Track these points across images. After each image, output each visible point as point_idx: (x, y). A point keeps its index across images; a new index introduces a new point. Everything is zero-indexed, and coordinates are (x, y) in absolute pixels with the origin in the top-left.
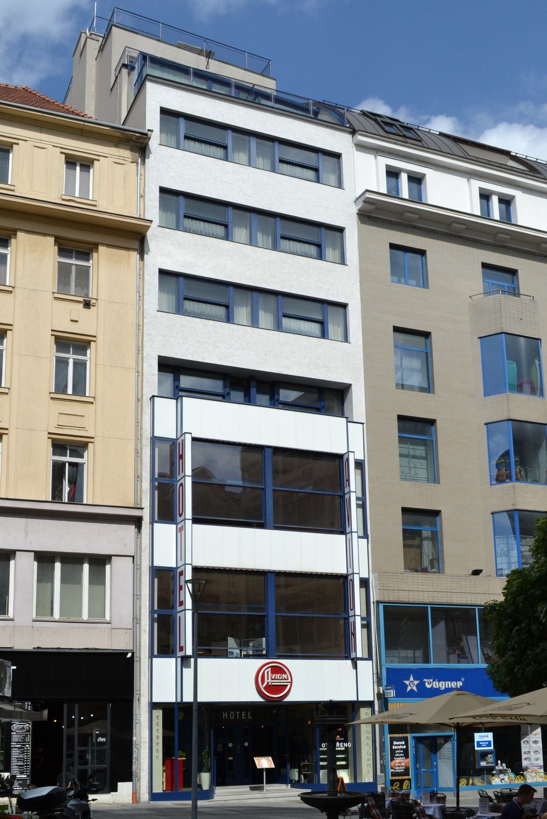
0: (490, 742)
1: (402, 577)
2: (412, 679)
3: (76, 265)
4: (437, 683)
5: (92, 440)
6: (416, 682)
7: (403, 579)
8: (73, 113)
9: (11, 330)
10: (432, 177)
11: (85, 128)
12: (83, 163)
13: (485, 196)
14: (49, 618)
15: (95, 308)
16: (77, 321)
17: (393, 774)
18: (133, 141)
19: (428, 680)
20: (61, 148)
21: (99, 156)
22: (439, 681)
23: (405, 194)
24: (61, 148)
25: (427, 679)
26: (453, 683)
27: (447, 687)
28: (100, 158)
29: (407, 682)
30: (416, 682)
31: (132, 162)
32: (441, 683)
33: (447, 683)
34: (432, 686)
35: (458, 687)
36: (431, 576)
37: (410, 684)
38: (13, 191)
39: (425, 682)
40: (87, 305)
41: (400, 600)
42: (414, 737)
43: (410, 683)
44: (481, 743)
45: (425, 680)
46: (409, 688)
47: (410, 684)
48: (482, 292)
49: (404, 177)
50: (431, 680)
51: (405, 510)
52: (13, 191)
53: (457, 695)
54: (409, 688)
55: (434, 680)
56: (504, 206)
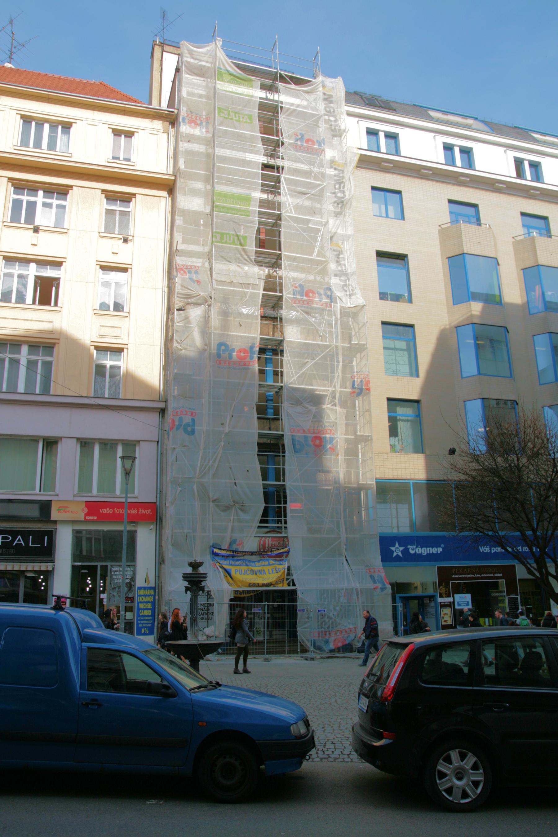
0: (468, 602)
1: (386, 457)
2: (397, 545)
3: (119, 211)
4: (420, 549)
5: (126, 346)
6: (401, 549)
7: (387, 458)
8: (136, 102)
9: (65, 262)
10: (404, 134)
11: (50, 97)
12: (127, 135)
13: (448, 148)
14: (89, 494)
15: (132, 243)
16: (117, 253)
17: (319, 637)
18: (163, 117)
19: (412, 547)
20: (17, 110)
21: (138, 129)
22: (421, 547)
23: (383, 149)
24: (17, 110)
25: (411, 545)
26: (434, 549)
27: (428, 552)
28: (139, 131)
29: (393, 549)
30: (401, 549)
31: (163, 133)
32: (423, 549)
33: (428, 549)
34: (416, 552)
35: (439, 552)
36: (412, 456)
37: (395, 550)
38: (133, 166)
39: (409, 548)
40: (126, 241)
41: (386, 476)
42: (400, 597)
44: (460, 603)
45: (409, 546)
46: (395, 554)
47: (395, 550)
48: (449, 221)
49: (382, 135)
50: (415, 547)
51: (389, 399)
52: (133, 166)
53: (147, 573)
54: (395, 554)
55: (417, 547)
56: (466, 156)
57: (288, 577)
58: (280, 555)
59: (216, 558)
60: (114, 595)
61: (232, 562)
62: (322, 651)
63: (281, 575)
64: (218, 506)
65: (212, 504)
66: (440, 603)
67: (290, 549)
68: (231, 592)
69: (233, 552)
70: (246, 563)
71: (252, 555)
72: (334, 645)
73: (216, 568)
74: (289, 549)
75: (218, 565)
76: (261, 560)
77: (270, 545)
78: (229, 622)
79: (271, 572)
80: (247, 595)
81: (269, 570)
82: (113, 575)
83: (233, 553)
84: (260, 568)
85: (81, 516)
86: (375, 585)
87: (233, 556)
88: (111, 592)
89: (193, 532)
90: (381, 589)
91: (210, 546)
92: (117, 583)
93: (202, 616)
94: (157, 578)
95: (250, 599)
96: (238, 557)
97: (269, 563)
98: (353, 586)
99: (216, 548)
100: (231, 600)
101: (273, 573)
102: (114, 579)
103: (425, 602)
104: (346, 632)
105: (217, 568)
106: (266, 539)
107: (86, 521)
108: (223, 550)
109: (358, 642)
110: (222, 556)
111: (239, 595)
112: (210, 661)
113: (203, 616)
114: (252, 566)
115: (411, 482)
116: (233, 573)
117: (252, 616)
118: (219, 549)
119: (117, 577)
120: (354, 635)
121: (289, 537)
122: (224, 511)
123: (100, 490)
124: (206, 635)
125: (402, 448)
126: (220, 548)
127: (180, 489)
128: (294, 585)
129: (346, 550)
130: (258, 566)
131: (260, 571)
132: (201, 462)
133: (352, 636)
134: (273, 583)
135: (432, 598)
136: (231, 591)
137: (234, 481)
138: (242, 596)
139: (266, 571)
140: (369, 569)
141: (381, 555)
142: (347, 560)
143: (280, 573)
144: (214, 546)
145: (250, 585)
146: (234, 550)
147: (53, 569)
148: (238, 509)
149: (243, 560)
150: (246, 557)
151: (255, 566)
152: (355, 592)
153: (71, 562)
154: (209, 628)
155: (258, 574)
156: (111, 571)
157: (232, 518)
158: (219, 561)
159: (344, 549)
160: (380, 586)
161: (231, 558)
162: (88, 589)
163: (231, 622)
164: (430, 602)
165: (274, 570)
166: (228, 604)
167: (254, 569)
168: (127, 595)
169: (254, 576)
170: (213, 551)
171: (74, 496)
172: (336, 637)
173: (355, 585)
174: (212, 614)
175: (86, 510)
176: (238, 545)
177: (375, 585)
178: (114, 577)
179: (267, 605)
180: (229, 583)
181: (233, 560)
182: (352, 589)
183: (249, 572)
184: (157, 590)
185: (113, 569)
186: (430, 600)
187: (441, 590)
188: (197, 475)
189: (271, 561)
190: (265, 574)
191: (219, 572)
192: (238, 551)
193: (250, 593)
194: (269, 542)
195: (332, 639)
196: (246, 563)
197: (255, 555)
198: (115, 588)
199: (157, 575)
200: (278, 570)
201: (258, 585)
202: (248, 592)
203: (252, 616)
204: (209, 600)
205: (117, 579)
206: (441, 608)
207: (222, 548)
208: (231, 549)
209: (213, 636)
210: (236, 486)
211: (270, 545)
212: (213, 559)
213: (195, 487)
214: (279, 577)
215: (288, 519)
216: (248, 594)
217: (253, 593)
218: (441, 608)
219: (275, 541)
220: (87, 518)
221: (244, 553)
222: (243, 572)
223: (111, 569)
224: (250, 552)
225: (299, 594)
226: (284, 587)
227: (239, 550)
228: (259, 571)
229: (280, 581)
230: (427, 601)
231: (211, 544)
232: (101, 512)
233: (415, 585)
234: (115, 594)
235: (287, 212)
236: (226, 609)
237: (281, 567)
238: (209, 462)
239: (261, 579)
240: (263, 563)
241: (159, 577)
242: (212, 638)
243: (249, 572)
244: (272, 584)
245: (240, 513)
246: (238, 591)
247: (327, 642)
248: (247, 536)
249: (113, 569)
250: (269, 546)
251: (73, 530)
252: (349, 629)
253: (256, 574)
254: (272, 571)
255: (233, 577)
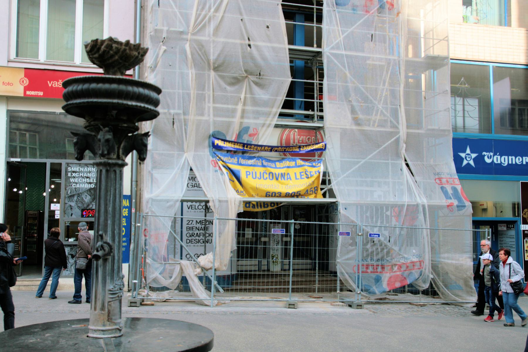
2: (468, 151)
6: (474, 155)
19: (488, 153)
25: (487, 152)
26: (517, 158)
27: (510, 162)
30: (474, 155)
33: (510, 158)
37: (466, 157)
39: (484, 155)
43: (467, 156)
47: (466, 157)
50: (492, 154)
57: (323, 187)
58: (311, 153)
59: (218, 153)
60: (71, 206)
61: (243, 161)
62: (370, 293)
63: (313, 182)
64: (222, 77)
65: (212, 73)
66: (524, 231)
67: (327, 146)
68: (240, 204)
69: (244, 145)
70: (262, 163)
71: (271, 151)
72: (388, 284)
73: (217, 168)
74: (326, 145)
75: (220, 163)
76: (283, 159)
77: (296, 141)
78: (236, 248)
79: (298, 176)
80: (264, 209)
81: (295, 173)
82: (70, 177)
83: (244, 146)
84: (283, 171)
85: (19, 90)
86: (450, 201)
87: (244, 152)
88: (67, 202)
89: (184, 114)
90: (458, 206)
91: (210, 137)
92: (75, 188)
93: (197, 238)
94: (134, 183)
95: (264, 214)
96: (250, 154)
97: (296, 164)
98: (419, 201)
99: (218, 139)
100: (239, 215)
101: (301, 178)
102: (71, 183)
103: (500, 228)
104: (407, 267)
105: (220, 167)
106: (290, 132)
107: (26, 99)
108: (229, 142)
109: (424, 282)
110: (228, 151)
111: (251, 209)
112: (206, 305)
113: (200, 238)
114: (271, 167)
115: (491, 65)
116: (243, 176)
117: (266, 239)
118: (222, 140)
119: (76, 180)
120: (419, 271)
121: (325, 127)
122: (232, 84)
123: (49, 54)
124: (200, 267)
125: (477, 21)
126: (224, 139)
127: (164, 48)
128: (332, 195)
129: (406, 150)
130: (280, 168)
131: (283, 175)
132: (197, 11)
133: (416, 274)
134: (302, 193)
135: (511, 224)
136: (240, 201)
137: (247, 42)
138: (256, 210)
139: (292, 176)
140: (440, 179)
141: (454, 160)
142: (407, 165)
143: (313, 179)
144: (215, 136)
145: (268, 195)
146: (245, 142)
147: (495, 321)
148: (252, 83)
149: (259, 158)
150: (263, 154)
151: (276, 168)
152: (421, 209)
153: (6, 158)
154: (205, 256)
155: (280, 179)
156: (67, 172)
157: (243, 96)
158: (222, 158)
159: (404, 149)
160: (456, 203)
161: (241, 154)
162: (15, 190)
163: (238, 247)
164: (507, 230)
165: (304, 174)
166: (234, 221)
167: (274, 172)
168: (91, 206)
169: (274, 181)
170: (213, 143)
171: (8, 61)
172: (392, 274)
173: (422, 200)
174: (211, 235)
175: (26, 82)
176: (250, 135)
177: (450, 201)
178: (72, 180)
179: (293, 225)
180: (237, 191)
181: (244, 158)
182: (417, 205)
183: (266, 176)
184: (134, 201)
185: (69, 169)
186: (507, 227)
187: (525, 214)
188: (191, 28)
189: (299, 162)
190: (291, 179)
191: (222, 173)
192: (251, 145)
193: (268, 206)
194: (295, 136)
195: (386, 277)
196: (262, 163)
197: (276, 151)
198: (73, 196)
199: (134, 179)
200: (309, 174)
201: (280, 195)
202: (265, 204)
203: (266, 239)
204: (207, 214)
205: (76, 183)
206: (524, 239)
207: (228, 139)
208: (240, 141)
209: (211, 268)
210: (250, 48)
211: (296, 141)
212: (214, 155)
213: (187, 47)
214: (310, 185)
215: (325, 101)
216: (264, 207)
217: (271, 206)
218: (524, 239)
219: (303, 136)
220: (28, 93)
221: (259, 148)
222: (258, 175)
223: (66, 169)
224: (269, 146)
225: (341, 208)
226: (318, 199)
227: (253, 143)
228: (282, 174)
229: (314, 191)
230: (502, 228)
231: (211, 132)
232: (50, 85)
233: (485, 207)
234: (73, 204)
235: (337, 47)
236: (231, 227)
237: (313, 170)
238: (209, 11)
239: (284, 186)
240: (287, 163)
241: (137, 181)
242: (209, 271)
243: (267, 176)
244: (300, 195)
245: (256, 88)
246: (249, 203)
247: (378, 280)
248: (263, 125)
249: (69, 169)
250: (294, 142)
251: (8, 111)
252: (411, 263)
253: (277, 179)
254: (301, 176)
255: (243, 182)
